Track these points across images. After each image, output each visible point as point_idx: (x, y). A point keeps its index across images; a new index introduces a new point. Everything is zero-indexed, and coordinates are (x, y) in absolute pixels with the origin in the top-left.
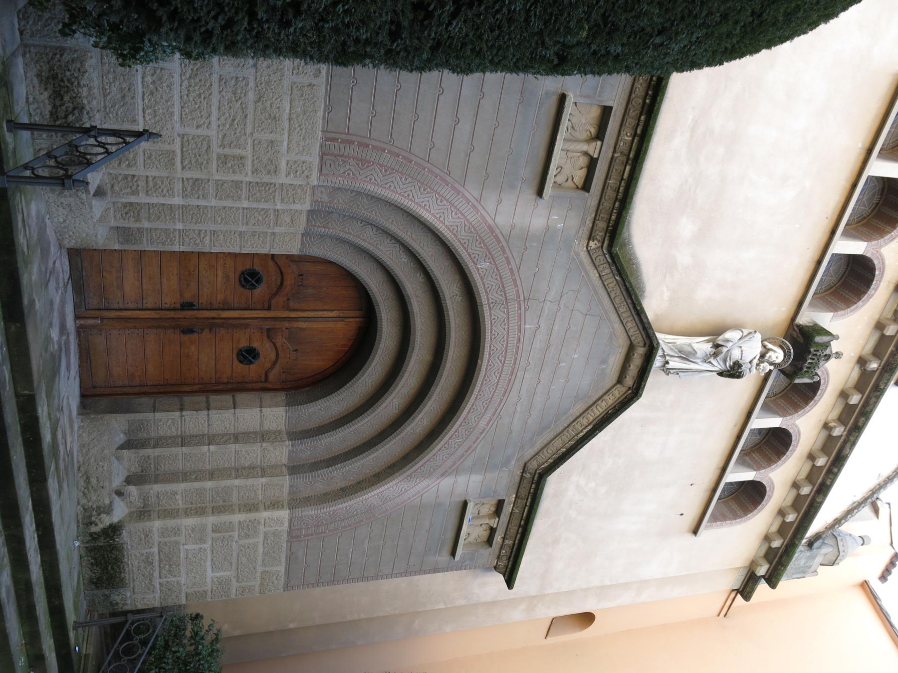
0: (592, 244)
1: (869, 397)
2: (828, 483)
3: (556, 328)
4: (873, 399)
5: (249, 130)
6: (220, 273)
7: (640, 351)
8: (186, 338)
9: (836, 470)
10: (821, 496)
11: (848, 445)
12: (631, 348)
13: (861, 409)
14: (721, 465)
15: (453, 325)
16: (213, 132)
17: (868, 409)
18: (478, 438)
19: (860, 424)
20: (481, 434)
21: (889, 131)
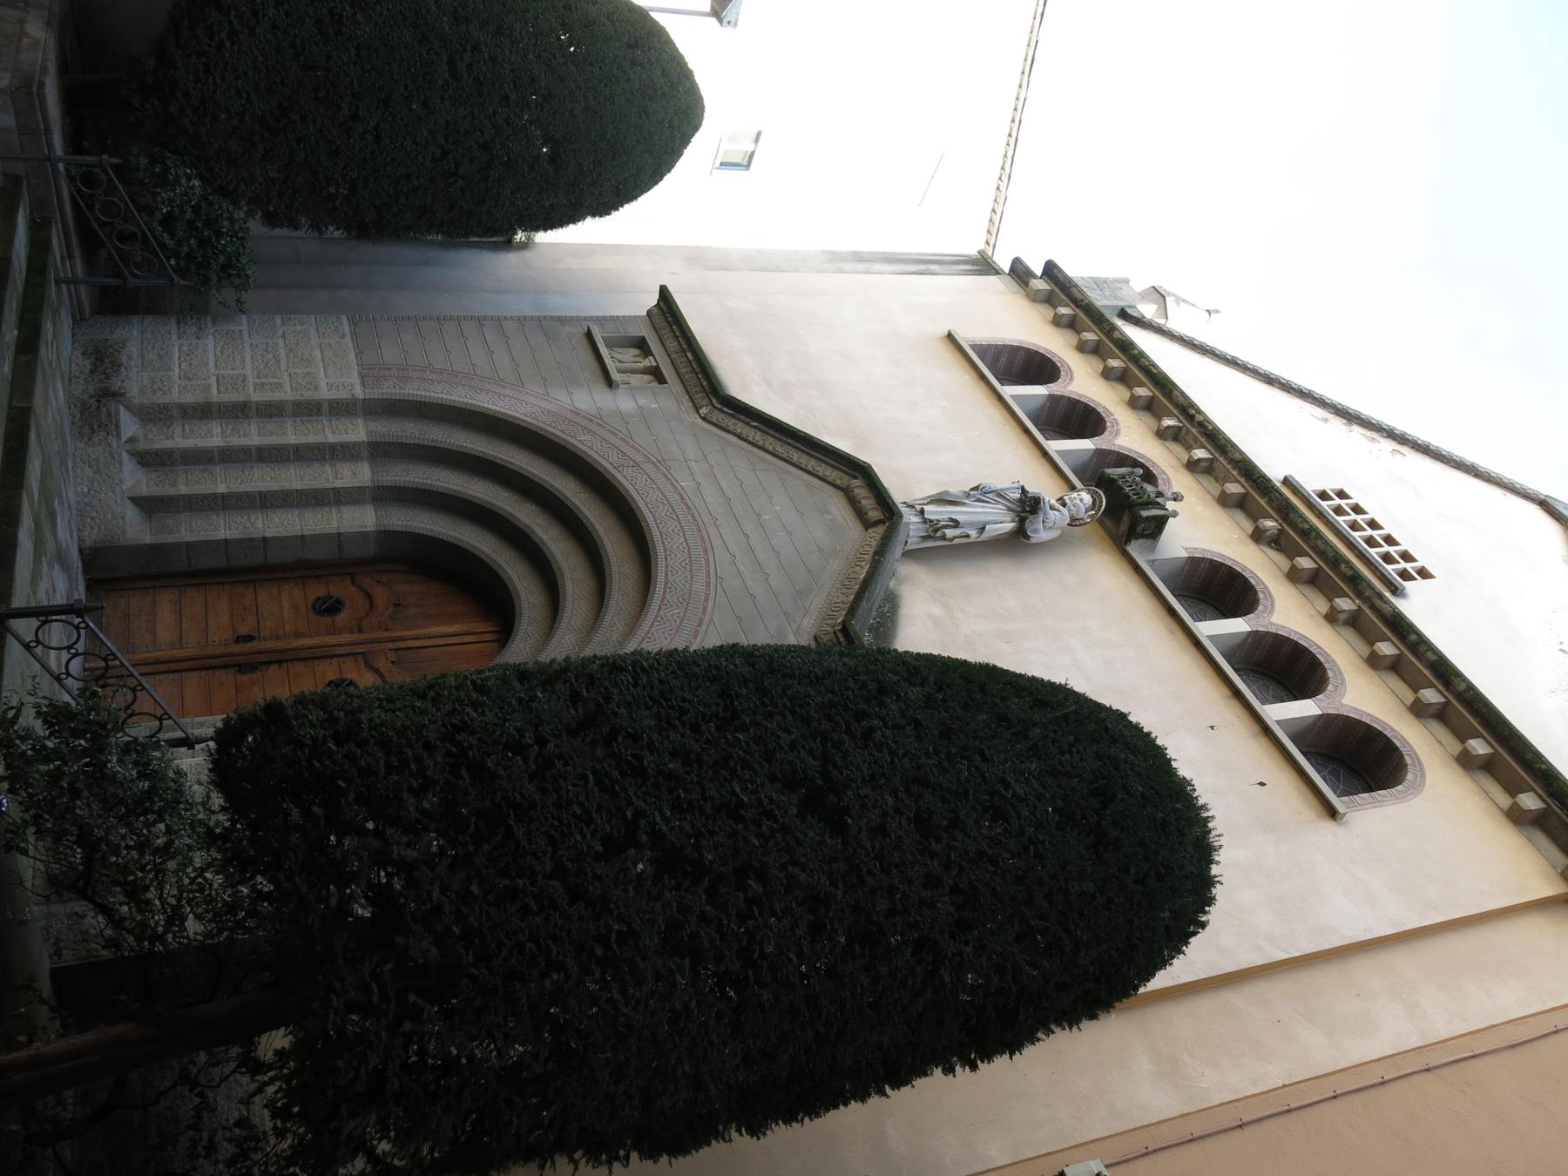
0: (703, 411)
1: (1177, 405)
2: (1434, 658)
3: (723, 483)
4: (1319, 543)
5: (283, 367)
6: (286, 604)
7: (861, 492)
8: (245, 678)
9: (1413, 637)
10: (1456, 681)
11: (1378, 602)
12: (847, 492)
13: (1326, 563)
14: (1226, 692)
15: (592, 519)
16: (248, 371)
17: (1330, 555)
18: (705, 608)
19: (1350, 573)
20: (706, 601)
21: (1324, 778)
